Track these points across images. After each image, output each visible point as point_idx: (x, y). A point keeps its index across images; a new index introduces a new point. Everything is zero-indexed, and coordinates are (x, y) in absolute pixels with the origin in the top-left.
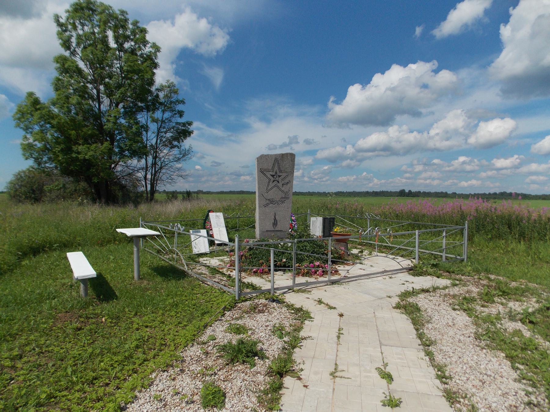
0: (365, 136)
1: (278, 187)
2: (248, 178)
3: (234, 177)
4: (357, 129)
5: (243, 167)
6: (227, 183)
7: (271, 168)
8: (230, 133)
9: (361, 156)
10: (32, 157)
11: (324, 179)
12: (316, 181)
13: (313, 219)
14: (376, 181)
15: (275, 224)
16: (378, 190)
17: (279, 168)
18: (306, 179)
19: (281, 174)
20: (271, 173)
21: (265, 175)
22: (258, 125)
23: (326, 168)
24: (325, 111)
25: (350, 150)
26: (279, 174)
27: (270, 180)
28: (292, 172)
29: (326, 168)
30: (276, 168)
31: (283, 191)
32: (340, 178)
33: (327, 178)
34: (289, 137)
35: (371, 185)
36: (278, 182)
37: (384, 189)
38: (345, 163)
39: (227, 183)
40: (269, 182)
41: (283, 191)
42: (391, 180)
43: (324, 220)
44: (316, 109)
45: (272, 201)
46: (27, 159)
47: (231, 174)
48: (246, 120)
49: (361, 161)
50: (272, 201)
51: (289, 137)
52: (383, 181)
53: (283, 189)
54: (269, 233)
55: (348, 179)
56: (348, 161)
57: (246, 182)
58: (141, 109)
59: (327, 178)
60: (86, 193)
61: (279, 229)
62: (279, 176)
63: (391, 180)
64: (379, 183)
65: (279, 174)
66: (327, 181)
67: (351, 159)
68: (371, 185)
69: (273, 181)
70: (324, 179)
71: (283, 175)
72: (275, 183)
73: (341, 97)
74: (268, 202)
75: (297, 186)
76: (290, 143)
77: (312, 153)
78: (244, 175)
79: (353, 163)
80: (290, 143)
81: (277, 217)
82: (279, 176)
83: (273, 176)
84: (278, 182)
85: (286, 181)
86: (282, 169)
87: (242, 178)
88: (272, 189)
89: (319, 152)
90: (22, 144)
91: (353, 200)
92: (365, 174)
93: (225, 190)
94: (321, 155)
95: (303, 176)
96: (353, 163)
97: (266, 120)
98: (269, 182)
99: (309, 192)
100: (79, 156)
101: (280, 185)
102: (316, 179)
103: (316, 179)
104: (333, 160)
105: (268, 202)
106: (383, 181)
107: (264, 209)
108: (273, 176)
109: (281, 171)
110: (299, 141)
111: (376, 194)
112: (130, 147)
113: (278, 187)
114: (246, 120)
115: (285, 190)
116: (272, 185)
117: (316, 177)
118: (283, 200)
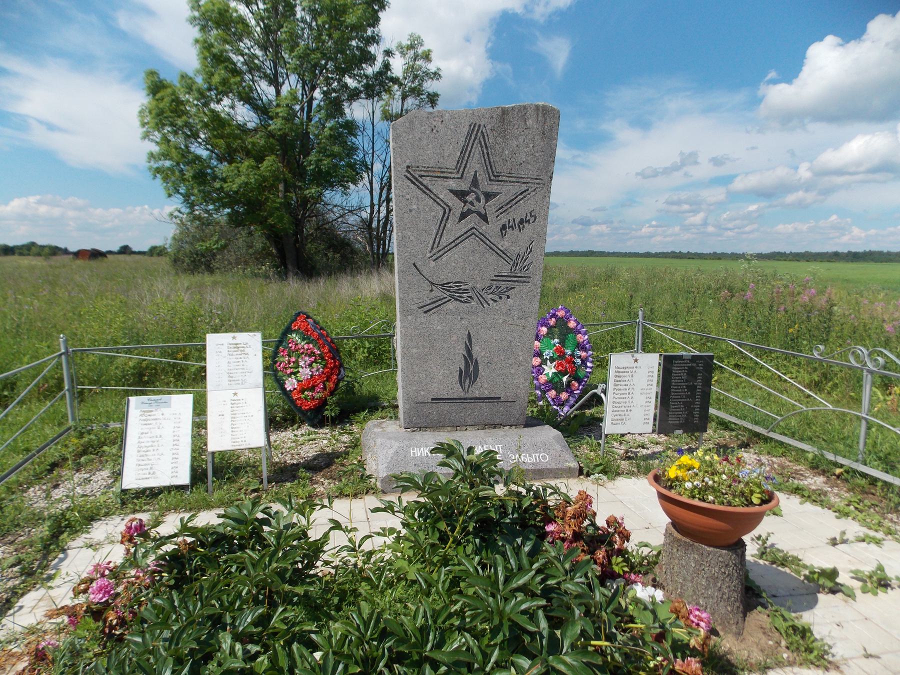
0: (837, 145)
1: (483, 238)
2: (604, 228)
3: (580, 227)
4: (820, 130)
5: (594, 210)
6: (567, 238)
7: (451, 164)
8: (576, 152)
9: (826, 181)
10: (178, 192)
11: (747, 229)
12: (730, 233)
13: (618, 360)
14: (856, 231)
15: (469, 371)
16: (860, 249)
17: (489, 164)
18: (710, 229)
19: (494, 188)
20: (453, 184)
21: (426, 190)
22: (625, 133)
23: (753, 207)
24: (756, 101)
25: (804, 173)
26: (486, 186)
27: (447, 211)
28: (544, 180)
29: (753, 207)
30: (475, 165)
31: (502, 254)
32: (780, 227)
33: (755, 226)
34: (681, 154)
35: (845, 239)
36: (484, 218)
37: (874, 247)
38: (791, 198)
39: (567, 238)
40: (445, 218)
41: (502, 254)
42: (892, 229)
43: (668, 363)
44: (741, 97)
45: (455, 291)
46: (170, 196)
47: (574, 222)
48: (605, 127)
49: (827, 192)
50: (455, 291)
51: (681, 154)
52: (873, 232)
53: (504, 244)
54: (445, 407)
55: (796, 229)
56: (800, 194)
57: (601, 235)
58: (354, 95)
59: (755, 226)
60: (261, 256)
61: (486, 394)
62: (489, 196)
63: (892, 229)
64: (863, 235)
65: (486, 186)
66: (752, 232)
67: (807, 190)
68: (845, 239)
69: (463, 216)
70: (747, 229)
71: (506, 191)
72: (472, 221)
73: (791, 69)
74: (438, 293)
75: (560, 235)
76: (683, 164)
77: (726, 180)
78: (597, 223)
79: (810, 197)
80: (683, 164)
81: (476, 350)
82: (489, 196)
83: (461, 195)
84: (484, 218)
85: (517, 214)
86: (498, 168)
87: (594, 228)
88: (456, 243)
89: (739, 178)
90: (150, 169)
91: (805, 270)
92: (834, 217)
93: (561, 249)
94: (739, 185)
95: (705, 224)
96: (810, 197)
97: (642, 124)
98: (445, 218)
99: (715, 253)
100: (225, 185)
101: (491, 229)
102: (730, 229)
103: (730, 229)
104: (764, 194)
105: (438, 293)
106: (873, 232)
107: (423, 318)
108: (461, 195)
109: (495, 177)
110: (699, 160)
111: (854, 257)
112: (317, 166)
113: (483, 238)
114: (605, 127)
115: (515, 250)
116: (455, 229)
117: (730, 225)
118: (504, 285)
